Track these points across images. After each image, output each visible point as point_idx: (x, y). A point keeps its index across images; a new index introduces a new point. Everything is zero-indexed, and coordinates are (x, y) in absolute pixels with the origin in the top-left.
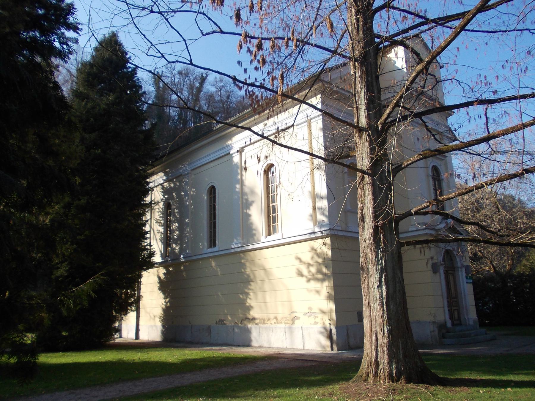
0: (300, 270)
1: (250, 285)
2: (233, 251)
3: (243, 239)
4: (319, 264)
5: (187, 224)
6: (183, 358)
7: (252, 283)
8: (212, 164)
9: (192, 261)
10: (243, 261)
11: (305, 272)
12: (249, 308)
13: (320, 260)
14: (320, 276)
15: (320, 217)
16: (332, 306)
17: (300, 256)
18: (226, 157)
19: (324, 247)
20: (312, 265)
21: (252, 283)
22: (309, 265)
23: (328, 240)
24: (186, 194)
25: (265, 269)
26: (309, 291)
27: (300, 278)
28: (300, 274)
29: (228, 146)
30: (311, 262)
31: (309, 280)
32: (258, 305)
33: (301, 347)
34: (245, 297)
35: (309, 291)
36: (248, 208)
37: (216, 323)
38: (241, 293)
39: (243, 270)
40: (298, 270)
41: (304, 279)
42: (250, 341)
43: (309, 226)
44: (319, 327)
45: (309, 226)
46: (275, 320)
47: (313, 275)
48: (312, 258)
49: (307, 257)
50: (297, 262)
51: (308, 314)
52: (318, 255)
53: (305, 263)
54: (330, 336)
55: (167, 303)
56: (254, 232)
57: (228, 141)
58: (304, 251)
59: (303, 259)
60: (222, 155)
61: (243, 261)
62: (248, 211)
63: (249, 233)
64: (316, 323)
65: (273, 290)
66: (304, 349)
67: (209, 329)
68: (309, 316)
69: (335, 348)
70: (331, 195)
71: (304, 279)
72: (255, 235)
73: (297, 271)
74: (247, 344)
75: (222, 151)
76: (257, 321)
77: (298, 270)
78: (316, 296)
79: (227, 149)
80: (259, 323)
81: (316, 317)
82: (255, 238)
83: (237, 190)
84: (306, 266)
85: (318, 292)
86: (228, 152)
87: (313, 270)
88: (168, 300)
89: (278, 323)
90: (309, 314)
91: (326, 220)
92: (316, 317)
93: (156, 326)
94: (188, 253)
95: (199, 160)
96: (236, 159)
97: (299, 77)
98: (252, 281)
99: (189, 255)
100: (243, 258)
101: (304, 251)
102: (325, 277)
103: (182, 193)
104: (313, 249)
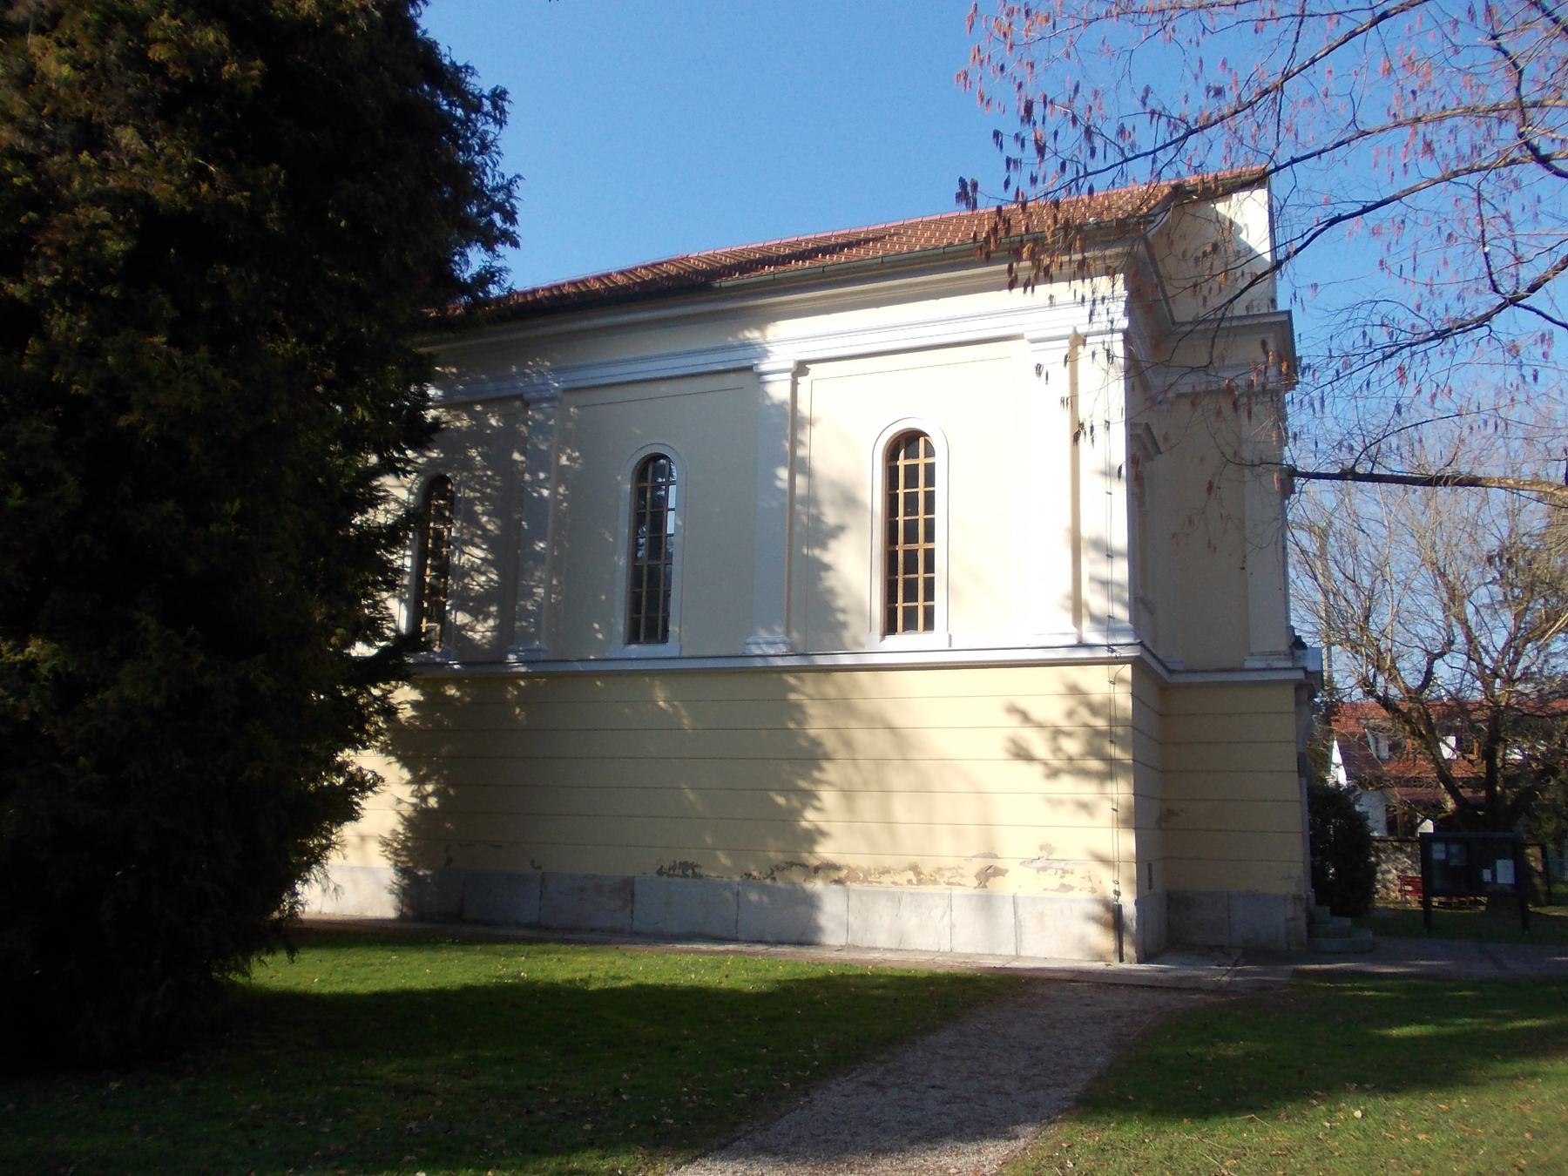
0: (1024, 745)
1: (821, 769)
2: (759, 663)
3: (788, 633)
4: (1097, 733)
5: (539, 557)
6: (782, 972)
7: (825, 764)
8: (664, 388)
9: (555, 677)
10: (793, 697)
11: (1039, 745)
12: (813, 837)
13: (1101, 723)
14: (1095, 764)
15: (1097, 602)
16: (1126, 843)
17: (1023, 703)
18: (733, 376)
19: (1111, 686)
20: (1069, 734)
21: (825, 764)
22: (1057, 733)
23: (1126, 671)
24: (539, 460)
25: (891, 728)
26: (1055, 803)
27: (1021, 766)
28: (1022, 754)
29: (748, 345)
30: (1064, 723)
31: (1054, 773)
32: (838, 828)
33: (1009, 950)
34: (796, 804)
35: (1055, 803)
36: (823, 545)
37: (660, 872)
38: (784, 791)
39: (792, 725)
40: (1014, 742)
41: (1036, 770)
42: (818, 929)
43: (1059, 630)
44: (1082, 901)
45: (1059, 630)
46: (911, 875)
47: (1070, 759)
48: (1070, 714)
49: (1053, 710)
50: (1014, 721)
51: (1038, 864)
52: (1094, 710)
53: (1040, 726)
54: (1115, 920)
55: (424, 798)
56: (841, 617)
57: (747, 328)
58: (1045, 694)
59: (1036, 713)
60: (721, 367)
61: (793, 697)
62: (817, 552)
63: (815, 612)
64: (1066, 888)
65: (923, 789)
66: (1018, 957)
67: (627, 889)
68: (1044, 869)
69: (1129, 950)
70: (1141, 550)
71: (1036, 770)
72: (844, 625)
73: (1009, 745)
74: (807, 937)
75: (716, 357)
76: (843, 874)
77: (1014, 742)
78: (1082, 818)
79: (750, 352)
80: (847, 878)
81: (1065, 872)
82: (847, 636)
83: (779, 484)
84: (1046, 734)
85: (1084, 806)
86: (746, 364)
87: (1072, 746)
88: (429, 788)
89: (920, 882)
90: (1045, 860)
91: (1122, 613)
92: (1065, 872)
93: (368, 870)
94: (538, 650)
95: (617, 363)
96: (778, 390)
97: (1307, 627)
98: (828, 758)
99: (543, 656)
100: (794, 690)
101: (1045, 694)
102: (1111, 772)
103: (517, 456)
104: (1074, 690)
